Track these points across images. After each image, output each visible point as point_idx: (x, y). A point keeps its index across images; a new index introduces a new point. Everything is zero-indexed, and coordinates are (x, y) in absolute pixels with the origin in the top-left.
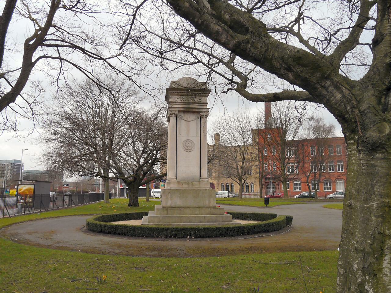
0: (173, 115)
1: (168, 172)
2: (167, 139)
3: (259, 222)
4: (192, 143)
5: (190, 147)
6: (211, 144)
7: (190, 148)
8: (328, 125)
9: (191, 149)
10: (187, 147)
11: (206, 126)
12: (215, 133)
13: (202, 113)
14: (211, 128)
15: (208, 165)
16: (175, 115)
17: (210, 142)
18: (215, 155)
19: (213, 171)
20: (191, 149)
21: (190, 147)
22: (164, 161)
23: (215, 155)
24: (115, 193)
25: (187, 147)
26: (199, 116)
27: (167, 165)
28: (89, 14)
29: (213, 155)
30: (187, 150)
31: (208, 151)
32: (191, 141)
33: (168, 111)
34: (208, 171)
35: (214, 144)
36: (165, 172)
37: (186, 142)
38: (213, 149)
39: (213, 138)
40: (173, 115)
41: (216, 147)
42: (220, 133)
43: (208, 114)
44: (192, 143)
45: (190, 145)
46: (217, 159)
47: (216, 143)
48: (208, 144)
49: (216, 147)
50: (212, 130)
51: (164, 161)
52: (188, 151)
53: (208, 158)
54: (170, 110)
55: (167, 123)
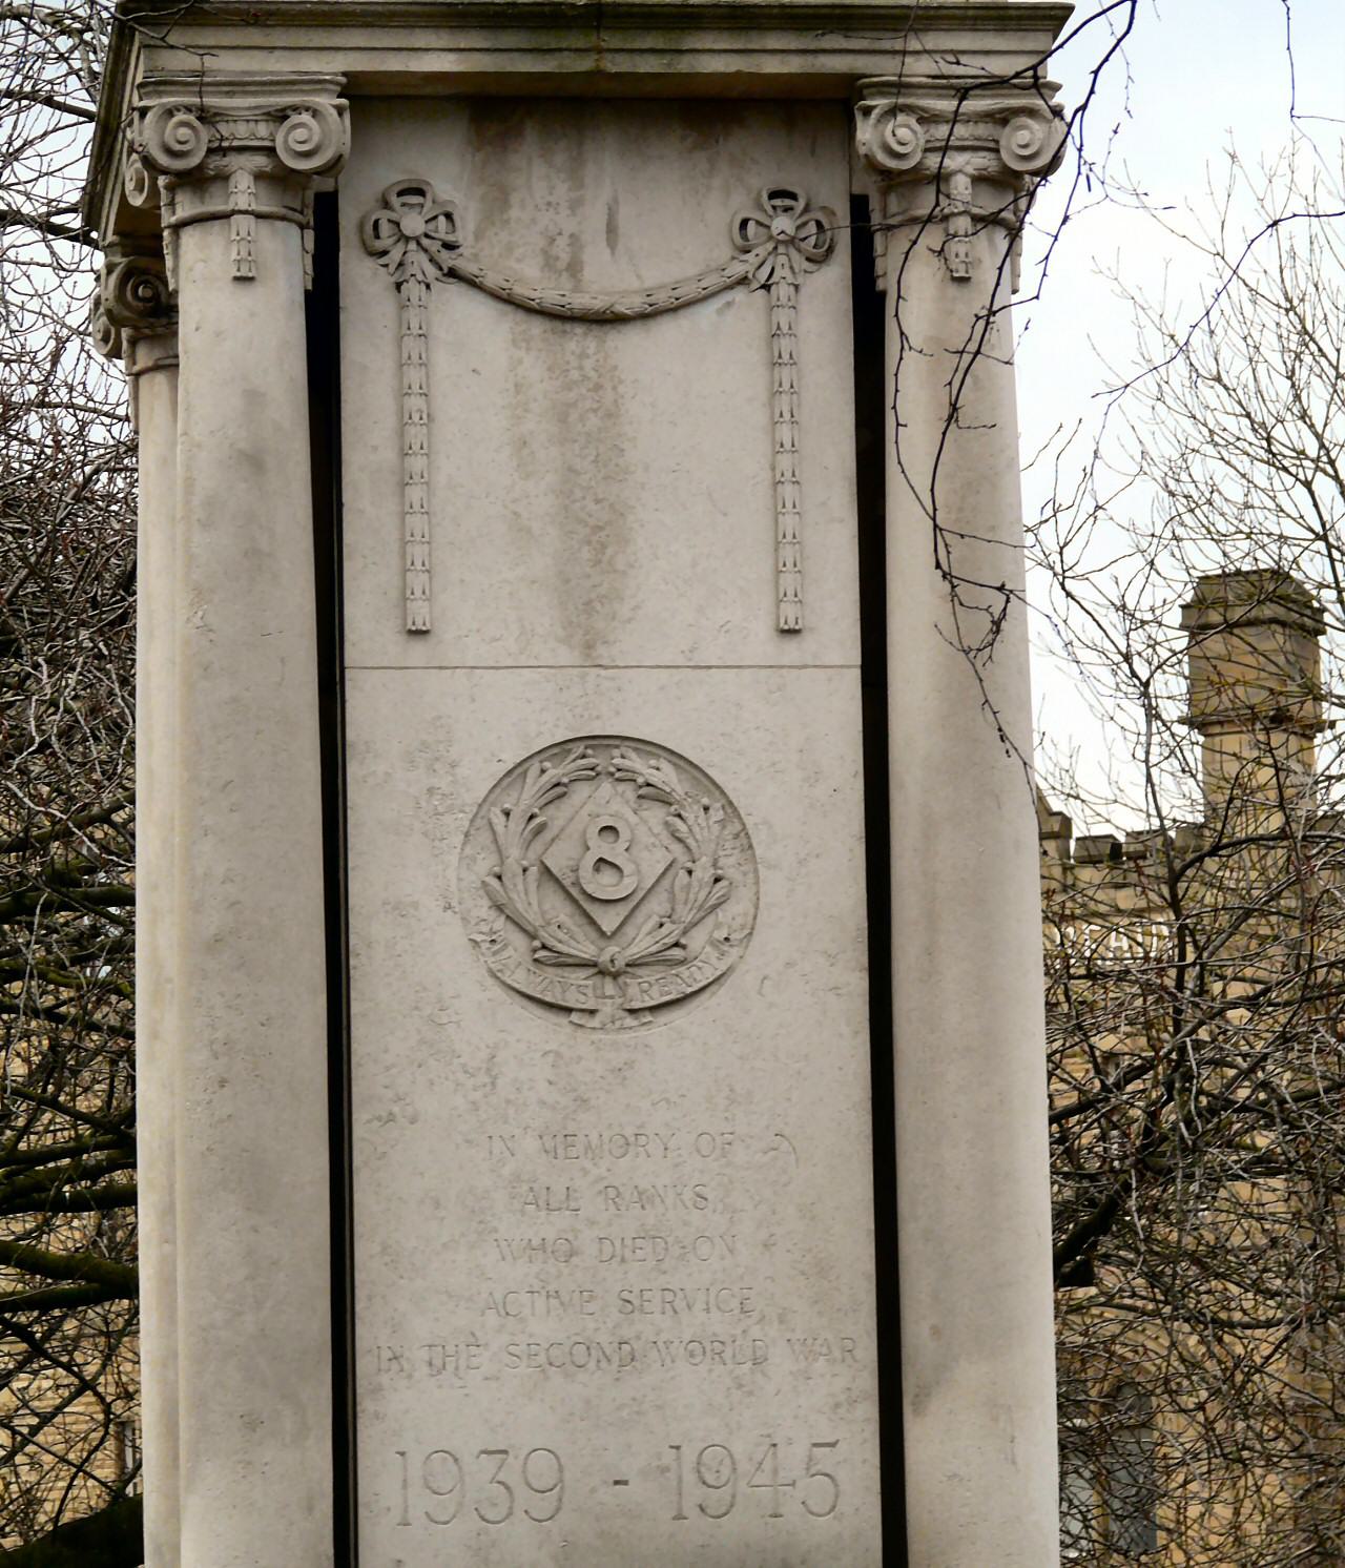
0: (243, 191)
1: (150, 1488)
2: (119, 731)
3: (989, 102)
4: (703, 828)
5: (633, 903)
6: (1125, 821)
7: (641, 941)
8: (1050, 78)
9: (672, 955)
10: (582, 903)
11: (996, 429)
12: (1208, 559)
13: (906, 134)
14: (1120, 456)
15: (1065, 1312)
16: (279, 178)
17: (1091, 781)
18: (1210, 1081)
19: (1177, 1430)
20: (672, 955)
21: (633, 903)
22: (68, 1235)
23: (1210, 1081)
24: (31, 977)
25: (582, 903)
26: (829, 190)
27: (118, 1339)
28: (1333, 356)
29: (1180, 1075)
30: (575, 988)
31: (1059, 970)
32: (666, 776)
33: (110, 87)
34: (1075, 1447)
35: (1183, 802)
36: (88, 1498)
37: (558, 791)
38: (1159, 936)
39: (1171, 688)
40: (243, 191)
41: (1245, 874)
42: (1313, 568)
43: (1025, 136)
44: (703, 828)
45: (652, 862)
46: (1265, 1165)
47: (1230, 796)
48: (1055, 828)
49: (1245, 874)
50: (1144, 505)
51: (68, 1235)
52: (608, 998)
53: (1063, 1144)
54: (156, 84)
55: (107, 381)
